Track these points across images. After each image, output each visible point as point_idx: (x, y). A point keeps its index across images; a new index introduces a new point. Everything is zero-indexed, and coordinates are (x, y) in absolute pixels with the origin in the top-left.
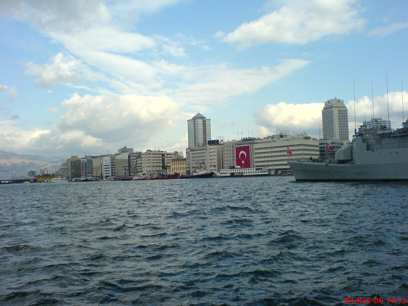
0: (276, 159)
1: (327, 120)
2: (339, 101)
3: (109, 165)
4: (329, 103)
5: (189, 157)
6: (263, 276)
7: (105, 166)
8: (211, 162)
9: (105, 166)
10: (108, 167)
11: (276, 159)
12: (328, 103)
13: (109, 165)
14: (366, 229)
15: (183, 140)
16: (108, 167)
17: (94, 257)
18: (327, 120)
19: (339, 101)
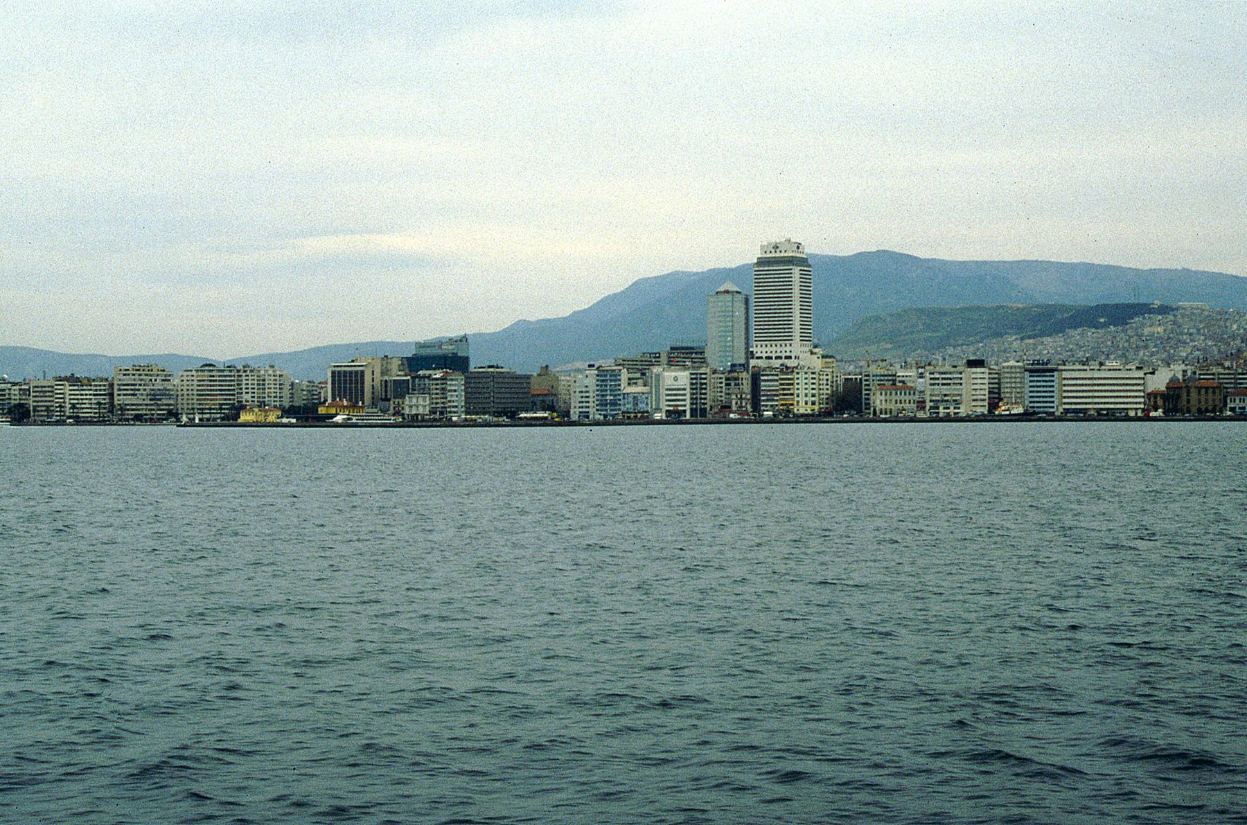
0: (1081, 394)
1: (787, 311)
2: (778, 247)
3: (685, 389)
4: (778, 250)
5: (920, 371)
6: (1198, 764)
7: (667, 390)
8: (974, 393)
9: (667, 390)
10: (684, 392)
11: (1081, 394)
12: (773, 251)
13: (685, 389)
14: (733, 789)
15: (1230, 269)
16: (684, 392)
17: (1149, 751)
18: (787, 311)
19: (778, 247)
